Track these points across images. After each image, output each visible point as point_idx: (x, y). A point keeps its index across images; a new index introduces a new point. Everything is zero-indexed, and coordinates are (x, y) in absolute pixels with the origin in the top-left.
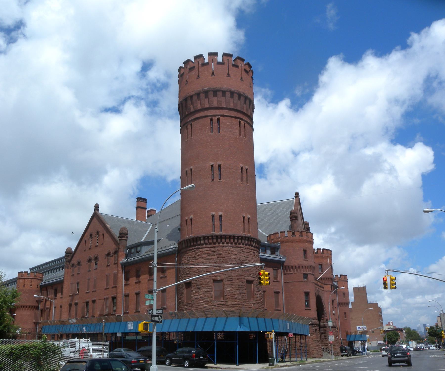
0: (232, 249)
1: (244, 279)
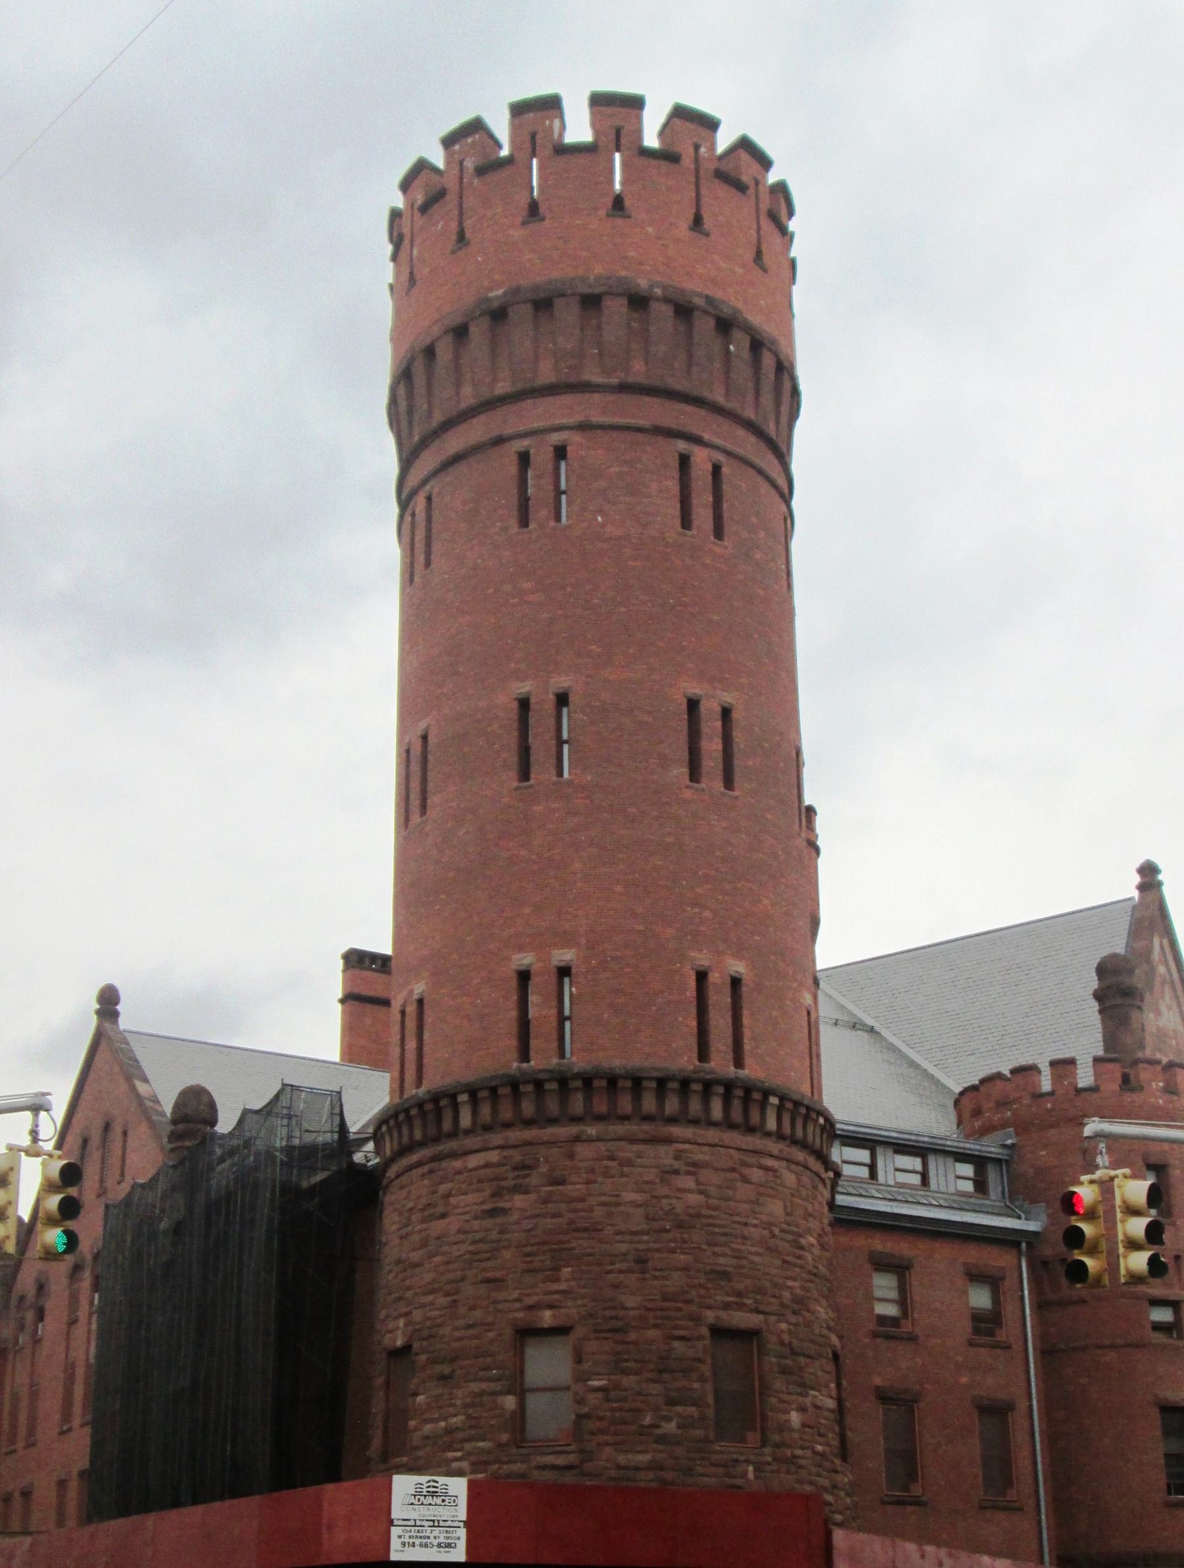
0: (628, 1151)
1: (697, 1319)
